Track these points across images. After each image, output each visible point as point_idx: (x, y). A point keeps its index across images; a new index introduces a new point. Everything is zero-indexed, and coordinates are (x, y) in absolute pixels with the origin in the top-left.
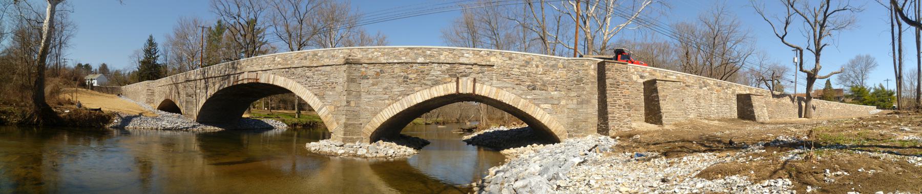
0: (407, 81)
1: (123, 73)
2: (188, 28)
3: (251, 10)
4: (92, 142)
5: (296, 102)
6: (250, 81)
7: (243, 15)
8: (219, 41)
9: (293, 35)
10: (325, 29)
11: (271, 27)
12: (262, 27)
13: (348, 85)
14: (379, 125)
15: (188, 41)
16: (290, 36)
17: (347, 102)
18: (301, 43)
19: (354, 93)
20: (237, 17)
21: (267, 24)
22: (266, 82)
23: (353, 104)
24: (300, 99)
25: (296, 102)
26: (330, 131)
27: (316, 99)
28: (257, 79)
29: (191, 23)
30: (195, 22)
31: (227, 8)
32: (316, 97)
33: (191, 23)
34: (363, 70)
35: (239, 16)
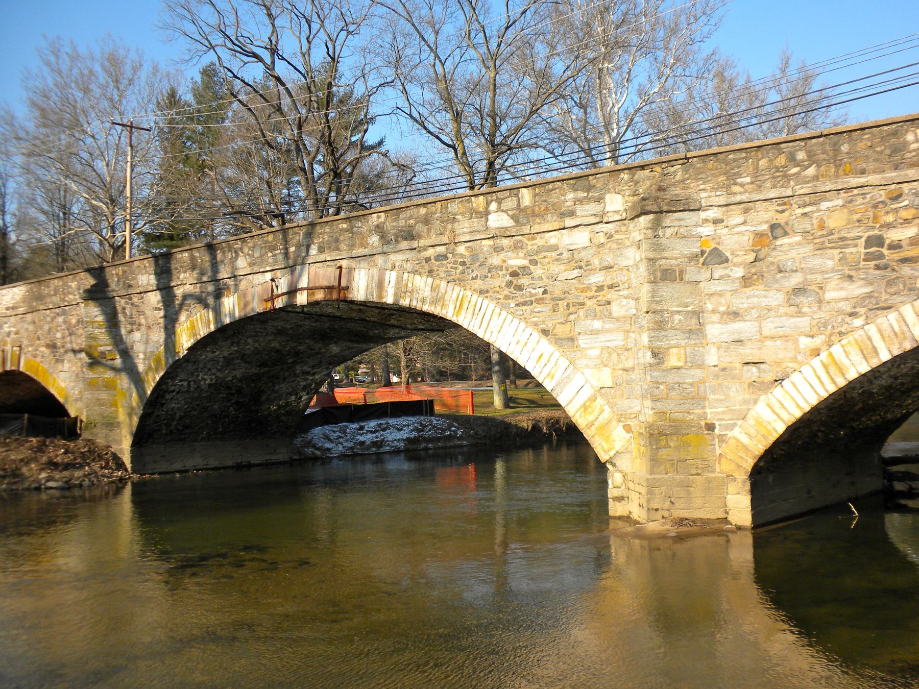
0: (882, 256)
1: (555, 218)
2: (86, 90)
3: (315, 26)
4: (86, 345)
5: (495, 357)
6: (320, 296)
7: (289, 45)
8: (211, 137)
9: (469, 111)
10: (581, 80)
11: (388, 90)
12: (360, 90)
13: (653, 294)
14: (781, 428)
15: (89, 140)
16: (457, 117)
17: (655, 355)
18: (498, 140)
19: (677, 317)
20: (266, 56)
21: (373, 81)
22: (374, 298)
23: (674, 359)
24: (502, 355)
25: (495, 357)
26: (603, 457)
27: (546, 346)
28: (340, 288)
29: (98, 68)
30: (114, 63)
31: (230, 19)
32: (544, 340)
33: (98, 68)
34: (707, 230)
35: (274, 51)
